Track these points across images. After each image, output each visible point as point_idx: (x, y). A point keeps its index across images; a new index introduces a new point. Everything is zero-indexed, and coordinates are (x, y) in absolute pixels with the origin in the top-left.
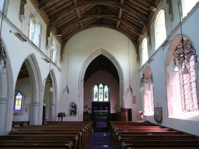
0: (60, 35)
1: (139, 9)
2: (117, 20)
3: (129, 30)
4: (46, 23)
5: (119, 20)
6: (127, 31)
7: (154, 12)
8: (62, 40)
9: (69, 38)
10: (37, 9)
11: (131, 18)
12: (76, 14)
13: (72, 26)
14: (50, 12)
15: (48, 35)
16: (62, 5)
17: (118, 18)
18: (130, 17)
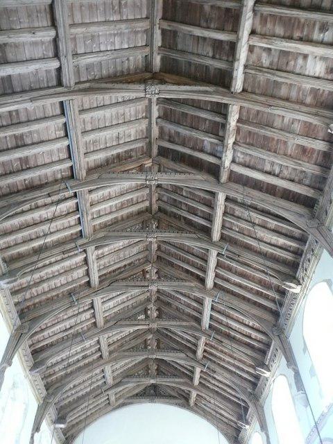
0: (62, 426)
1: (234, 370)
2: (190, 389)
3: (217, 412)
4: (38, 399)
5: (195, 388)
6: (214, 413)
7: (295, 296)
8: (65, 435)
9: (80, 431)
10: (28, 371)
11: (220, 385)
12: (99, 350)
13: (91, 402)
14: (50, 375)
15: (37, 428)
16: (78, 361)
17: (192, 386)
18: (217, 383)
